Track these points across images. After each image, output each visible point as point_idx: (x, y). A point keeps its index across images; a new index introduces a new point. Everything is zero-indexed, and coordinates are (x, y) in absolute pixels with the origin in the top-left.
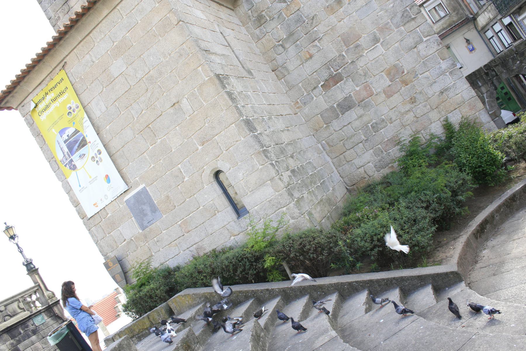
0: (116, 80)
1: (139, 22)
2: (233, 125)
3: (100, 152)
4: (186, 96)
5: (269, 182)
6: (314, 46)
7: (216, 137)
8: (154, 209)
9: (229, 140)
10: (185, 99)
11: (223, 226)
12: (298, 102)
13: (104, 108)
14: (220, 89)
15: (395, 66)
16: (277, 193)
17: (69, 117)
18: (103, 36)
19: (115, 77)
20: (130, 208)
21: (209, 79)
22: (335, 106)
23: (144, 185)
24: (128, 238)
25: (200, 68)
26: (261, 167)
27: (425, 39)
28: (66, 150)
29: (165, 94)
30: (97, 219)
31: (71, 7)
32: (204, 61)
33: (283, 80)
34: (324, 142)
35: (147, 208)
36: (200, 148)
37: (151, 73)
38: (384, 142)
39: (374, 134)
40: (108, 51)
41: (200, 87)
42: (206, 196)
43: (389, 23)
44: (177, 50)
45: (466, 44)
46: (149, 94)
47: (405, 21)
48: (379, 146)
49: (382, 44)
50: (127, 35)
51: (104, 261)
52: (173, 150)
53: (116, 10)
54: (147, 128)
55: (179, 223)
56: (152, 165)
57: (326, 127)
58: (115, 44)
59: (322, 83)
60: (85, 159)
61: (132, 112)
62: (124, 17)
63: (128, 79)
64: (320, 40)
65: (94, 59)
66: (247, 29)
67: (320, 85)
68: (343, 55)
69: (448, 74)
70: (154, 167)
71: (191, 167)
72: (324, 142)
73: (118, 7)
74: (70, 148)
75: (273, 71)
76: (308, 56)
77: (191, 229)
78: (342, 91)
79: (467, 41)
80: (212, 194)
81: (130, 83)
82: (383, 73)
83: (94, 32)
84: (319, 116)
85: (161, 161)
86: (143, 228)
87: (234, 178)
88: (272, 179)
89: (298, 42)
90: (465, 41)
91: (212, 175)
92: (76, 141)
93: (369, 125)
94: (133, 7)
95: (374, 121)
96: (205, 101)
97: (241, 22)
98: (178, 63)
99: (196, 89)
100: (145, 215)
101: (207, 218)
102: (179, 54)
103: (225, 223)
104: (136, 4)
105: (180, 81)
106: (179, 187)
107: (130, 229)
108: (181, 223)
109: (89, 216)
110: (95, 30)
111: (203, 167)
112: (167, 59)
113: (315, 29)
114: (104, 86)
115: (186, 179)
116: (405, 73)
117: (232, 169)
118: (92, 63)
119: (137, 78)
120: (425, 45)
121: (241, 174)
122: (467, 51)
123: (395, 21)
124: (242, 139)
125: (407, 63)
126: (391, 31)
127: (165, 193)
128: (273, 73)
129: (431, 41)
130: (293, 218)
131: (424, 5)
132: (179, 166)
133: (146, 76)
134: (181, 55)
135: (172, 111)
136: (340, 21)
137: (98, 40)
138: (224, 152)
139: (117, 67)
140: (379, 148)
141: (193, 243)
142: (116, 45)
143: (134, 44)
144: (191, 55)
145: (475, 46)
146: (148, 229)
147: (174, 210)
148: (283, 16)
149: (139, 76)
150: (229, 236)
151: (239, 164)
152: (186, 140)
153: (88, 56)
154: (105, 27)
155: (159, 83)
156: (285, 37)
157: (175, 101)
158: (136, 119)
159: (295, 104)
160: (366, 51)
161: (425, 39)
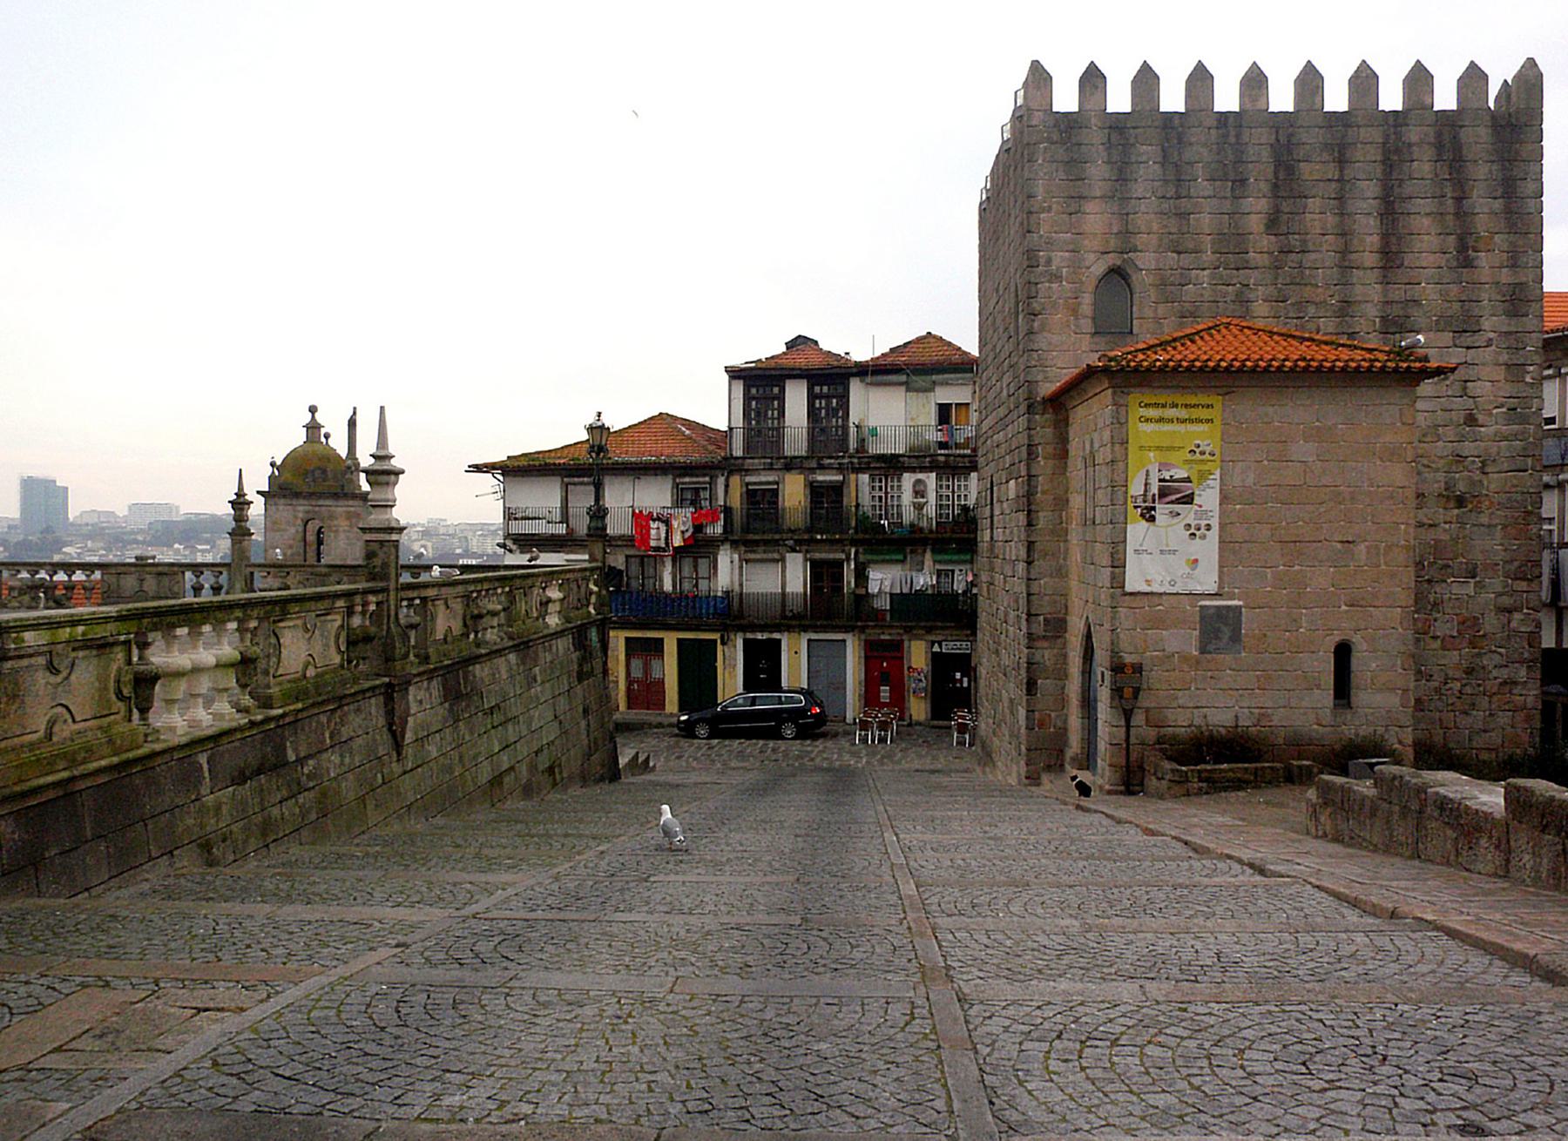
3: (1208, 527)
8: (1236, 638)
13: (1250, 480)
17: (1189, 456)
20: (1202, 618)
24: (1169, 650)
28: (1155, 490)
30: (1137, 602)
35: (1226, 633)
51: (446, 504)
60: (1176, 520)
74: (1163, 493)
87: (1361, 662)
88: (1406, 691)
92: (1178, 491)
100: (1217, 638)
107: (1183, 640)
109: (1128, 588)
123: (1508, 567)
125: (1491, 623)
130: (1400, 742)
149: (1324, 482)
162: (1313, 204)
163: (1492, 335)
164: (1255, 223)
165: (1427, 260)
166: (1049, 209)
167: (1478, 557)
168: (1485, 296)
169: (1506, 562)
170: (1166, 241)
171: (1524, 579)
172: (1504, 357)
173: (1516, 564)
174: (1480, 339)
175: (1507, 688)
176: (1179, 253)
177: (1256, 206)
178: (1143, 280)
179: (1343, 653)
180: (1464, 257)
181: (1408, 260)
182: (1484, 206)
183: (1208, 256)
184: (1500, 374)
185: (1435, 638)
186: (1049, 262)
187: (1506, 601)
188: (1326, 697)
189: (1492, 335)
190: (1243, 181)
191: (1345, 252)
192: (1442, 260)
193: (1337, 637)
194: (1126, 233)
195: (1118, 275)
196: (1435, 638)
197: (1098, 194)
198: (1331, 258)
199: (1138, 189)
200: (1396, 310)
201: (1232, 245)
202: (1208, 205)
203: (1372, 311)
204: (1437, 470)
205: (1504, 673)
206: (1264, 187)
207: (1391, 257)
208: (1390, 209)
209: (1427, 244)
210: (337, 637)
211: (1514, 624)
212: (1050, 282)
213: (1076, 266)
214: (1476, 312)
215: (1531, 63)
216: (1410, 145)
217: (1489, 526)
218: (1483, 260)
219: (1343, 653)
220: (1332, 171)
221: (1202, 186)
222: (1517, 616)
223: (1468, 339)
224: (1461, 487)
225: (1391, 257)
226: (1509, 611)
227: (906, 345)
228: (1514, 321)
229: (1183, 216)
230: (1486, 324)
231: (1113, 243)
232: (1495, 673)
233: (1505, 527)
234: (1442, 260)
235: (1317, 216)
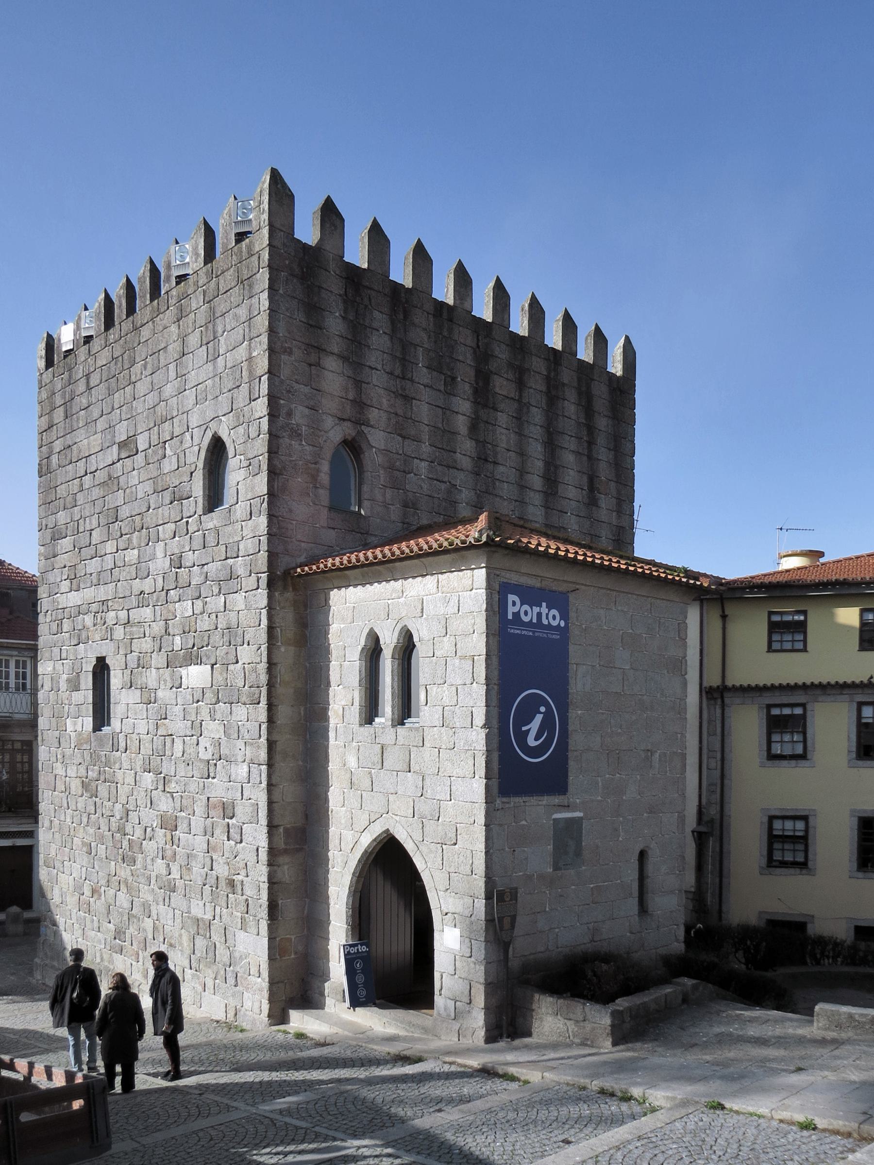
8: (578, 853)
23: (581, 814)
86: (556, 868)
146: (559, 873)
164: (461, 424)
166: (290, 353)
168: (603, 533)
170: (393, 421)
176: (404, 437)
178: (373, 458)
180: (592, 502)
182: (603, 454)
183: (426, 448)
186: (290, 414)
190: (454, 379)
195: (353, 447)
198: (513, 475)
201: (444, 436)
202: (426, 395)
207: (551, 481)
208: (551, 444)
209: (572, 487)
210: (586, 339)
212: (291, 437)
213: (315, 426)
215: (375, 220)
216: (564, 385)
225: (551, 481)
229: (407, 399)
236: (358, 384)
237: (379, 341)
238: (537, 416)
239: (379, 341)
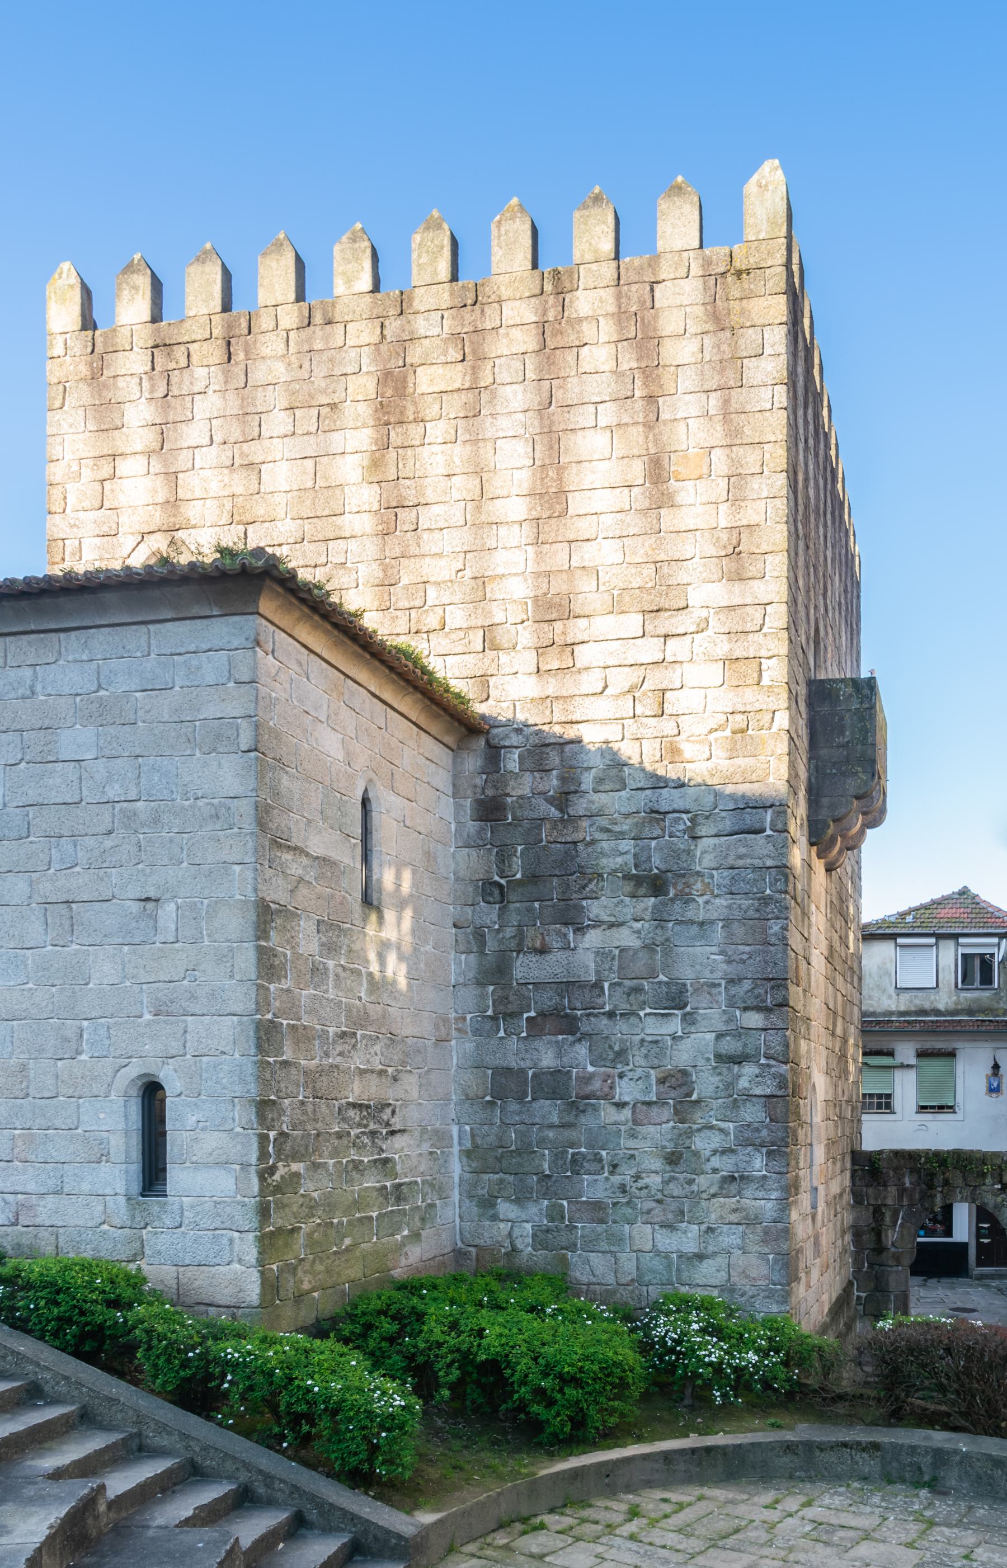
0: (59, 766)
1: (177, 688)
2: (235, 1018)
4: (180, 901)
5: (238, 1167)
6: (558, 933)
7: (190, 1018)
9: (210, 1042)
10: (172, 906)
11: (100, 1192)
12: (464, 1019)
14: (250, 932)
15: (684, 1073)
16: (239, 1197)
18: (85, 658)
19: (62, 757)
21: (241, 901)
22: (530, 1073)
25: (237, 868)
26: (239, 1130)
27: (763, 1061)
29: (140, 866)
31: (118, 473)
32: (253, 860)
33: (463, 956)
34: (467, 1128)
36: (147, 1017)
37: (139, 804)
38: (577, 1202)
39: (569, 1174)
40: (77, 695)
41: (216, 902)
42: (102, 1116)
43: (719, 985)
44: (216, 801)
45: (990, 1072)
46: (108, 843)
47: (749, 1003)
48: (565, 1203)
49: (684, 1015)
50: (138, 694)
52: (91, 985)
53: (143, 628)
54: (65, 906)
55: (17, 1132)
56: (30, 985)
57: (488, 1102)
58: (102, 693)
59: (533, 1014)
61: (53, 851)
62: (153, 656)
63: (84, 783)
64: (578, 929)
65: (38, 688)
66: (458, 807)
67: (525, 1015)
68: (602, 989)
69: (764, 1150)
70: (31, 989)
71: (107, 1042)
72: (467, 1128)
73: (151, 627)
75: (455, 926)
76: (538, 945)
77: (33, 1158)
78: (559, 1055)
79: (996, 1067)
80: (117, 1123)
81: (85, 793)
82: (652, 1072)
83: (73, 634)
84: (490, 1072)
85: (54, 989)
88: (244, 1166)
89: (537, 905)
90: (992, 1063)
91: (140, 1083)
93: (571, 1151)
94: (182, 650)
95: (583, 1150)
96: (209, 936)
97: (454, 785)
98: (201, 827)
99: (206, 901)
101: (78, 1159)
102: (213, 812)
103: (108, 1191)
104: (192, 648)
105: (185, 864)
106: (60, 1063)
108: (19, 1135)
110: (77, 632)
111: (130, 1057)
112: (187, 803)
113: (584, 903)
114: (27, 758)
115: (84, 1057)
116: (695, 1097)
117: (183, 1097)
118: (28, 692)
119: (103, 792)
120: (757, 1071)
121: (194, 1118)
122: (984, 1088)
123: (733, 991)
124: (237, 1056)
125: (706, 1083)
126: (715, 1005)
127: (22, 1056)
128: (454, 930)
129: (773, 1070)
131: (961, 940)
132: (85, 1023)
133: (125, 804)
134: (217, 817)
135: (135, 907)
136: (636, 920)
137: (70, 658)
138: (188, 1056)
139: (77, 739)
140: (562, 1206)
141: (20, 1189)
142: (101, 698)
143: (140, 724)
144: (236, 830)
145: (1004, 1088)
147: (19, 1101)
148: (540, 834)
150: (101, 1221)
151: (203, 1097)
152: (128, 984)
153: (28, 672)
154: (101, 643)
155: (141, 836)
156: (519, 876)
157: (152, 894)
158: (52, 870)
159: (456, 1019)
160: (648, 1010)
161: (763, 1061)
162: (437, 431)
163: (704, 613)
165: (604, 500)
167: (686, 973)
169: (731, 981)
171: (758, 1009)
172: (723, 648)
173: (747, 985)
174: (684, 623)
175: (734, 1188)
177: (357, 438)
179: (152, 1093)
181: (576, 504)
184: (714, 673)
185: (621, 1105)
187: (730, 1046)
188: (118, 1175)
189: (704, 613)
191: (482, 496)
192: (620, 499)
193: (134, 1070)
194: (173, 503)
196: (621, 1105)
197: (139, 448)
199: (194, 434)
200: (559, 585)
203: (519, 589)
204: (620, 836)
205: (725, 1165)
206: (365, 410)
207: (552, 500)
208: (551, 437)
209: (602, 465)
211: (743, 1083)
214: (683, 577)
216: (580, 320)
217: (702, 924)
218: (686, 492)
219: (152, 1093)
220: (456, 377)
221: (278, 422)
222: (749, 1070)
223: (667, 623)
224: (657, 862)
225: (552, 500)
226: (737, 1060)
227: (847, 562)
228: (737, 586)
230: (696, 597)
231: (158, 518)
232: (716, 1162)
233: (728, 922)
234: (620, 499)
235: (436, 456)
236: (172, 477)
237: (208, 405)
238: (515, 399)
239: (208, 405)
